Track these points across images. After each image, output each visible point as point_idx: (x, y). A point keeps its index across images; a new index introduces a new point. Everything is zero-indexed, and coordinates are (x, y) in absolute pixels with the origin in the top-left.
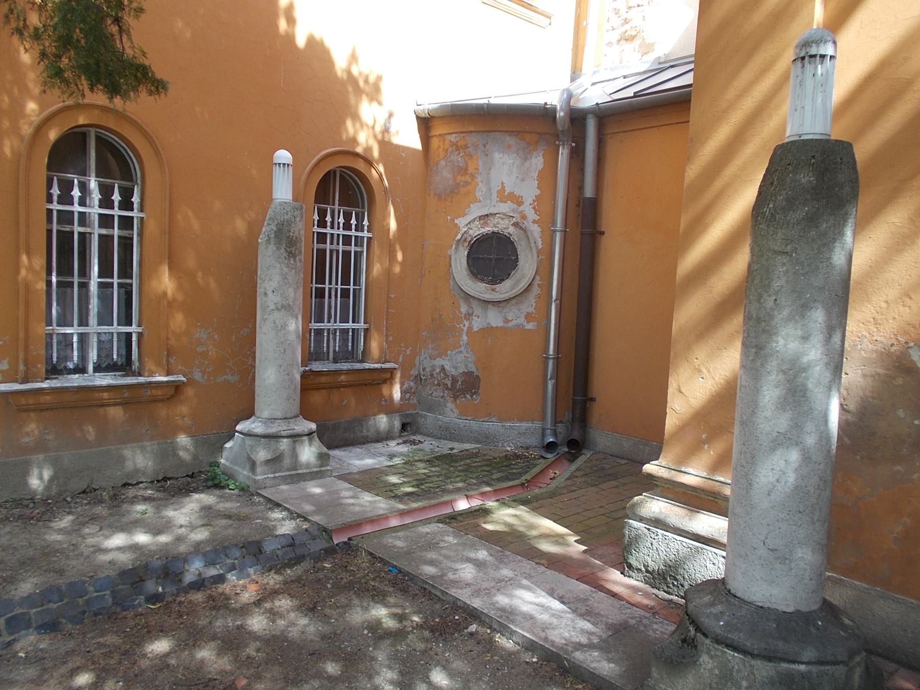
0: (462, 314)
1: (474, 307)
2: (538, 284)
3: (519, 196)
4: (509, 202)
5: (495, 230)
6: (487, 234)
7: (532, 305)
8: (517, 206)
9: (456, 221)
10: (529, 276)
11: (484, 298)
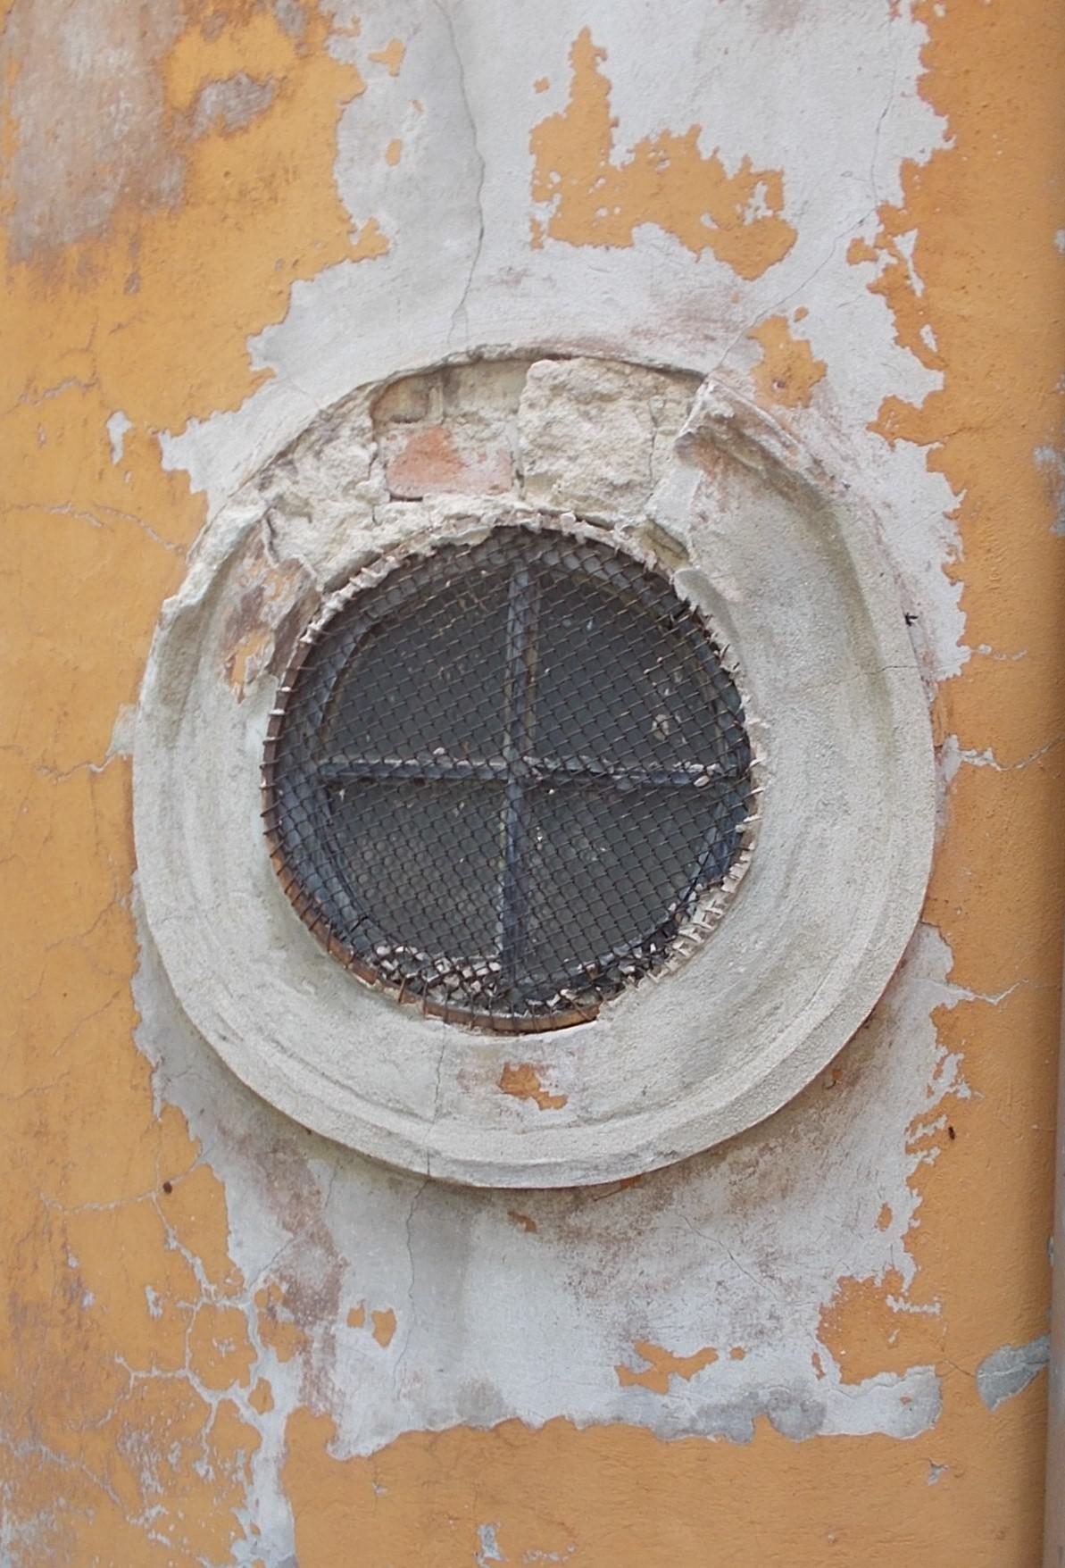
0: (234, 1291)
1: (344, 1232)
2: (939, 1015)
3: (748, 178)
4: (650, 233)
5: (525, 506)
6: (445, 548)
7: (886, 1215)
8: (725, 274)
9: (176, 454)
10: (862, 939)
11: (431, 1155)
